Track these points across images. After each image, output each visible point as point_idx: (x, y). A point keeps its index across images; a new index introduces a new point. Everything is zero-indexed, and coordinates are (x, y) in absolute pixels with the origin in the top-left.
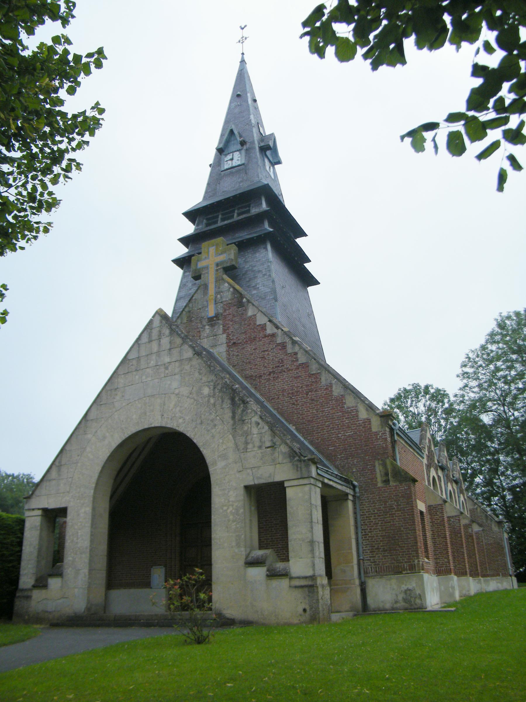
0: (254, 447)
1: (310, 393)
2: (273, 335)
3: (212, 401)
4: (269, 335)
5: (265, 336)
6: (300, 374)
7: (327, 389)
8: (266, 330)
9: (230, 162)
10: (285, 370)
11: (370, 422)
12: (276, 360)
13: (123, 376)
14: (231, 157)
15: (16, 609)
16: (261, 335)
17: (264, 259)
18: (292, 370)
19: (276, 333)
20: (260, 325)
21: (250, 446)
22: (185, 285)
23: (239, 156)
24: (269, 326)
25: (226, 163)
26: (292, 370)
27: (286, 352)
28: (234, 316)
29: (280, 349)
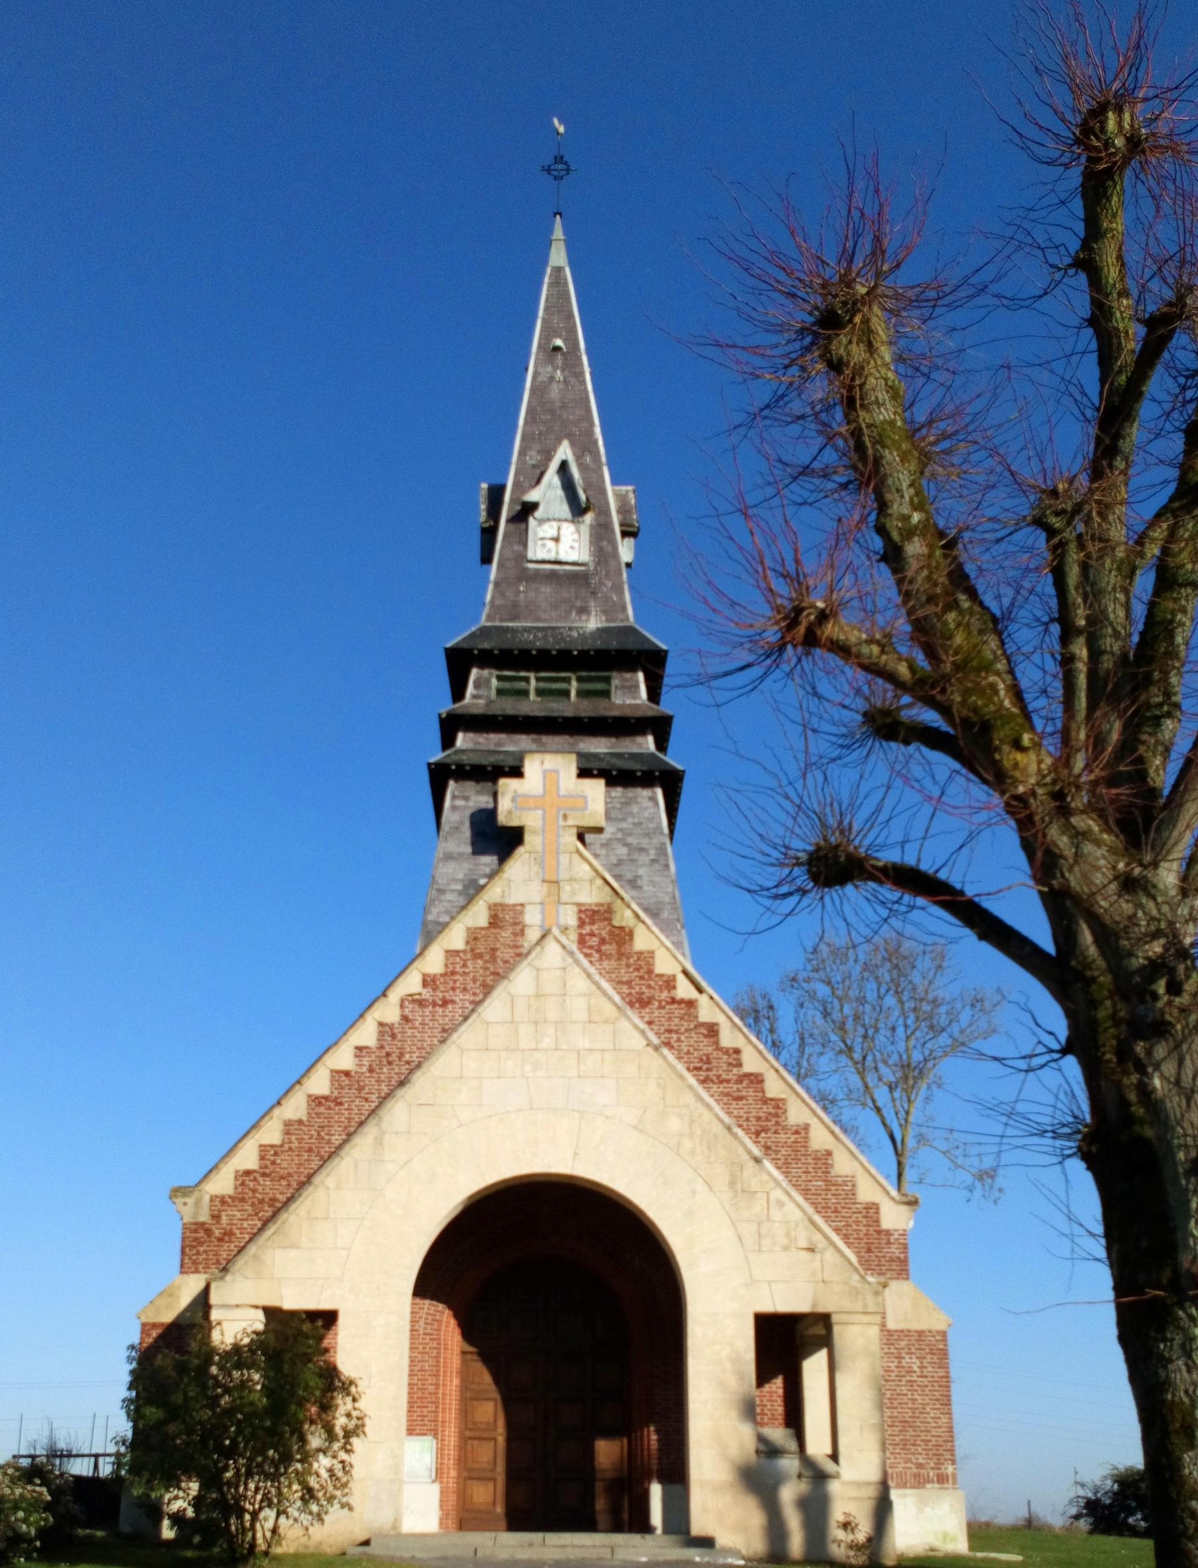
0: (774, 1244)
1: (763, 1135)
2: (691, 1004)
3: (687, 1144)
4: (681, 1001)
5: (673, 1001)
6: (744, 1094)
7: (797, 1132)
8: (674, 988)
9: (551, 544)
10: (714, 1079)
11: (878, 1208)
12: (696, 1054)
13: (474, 1054)
14: (554, 533)
15: (406, 1469)
16: (665, 995)
17: (651, 825)
18: (728, 1081)
19: (696, 1001)
20: (662, 975)
21: (766, 1243)
22: (457, 828)
23: (576, 536)
24: (682, 981)
25: (540, 542)
26: (728, 1081)
27: (717, 1043)
28: (603, 941)
29: (705, 1036)
